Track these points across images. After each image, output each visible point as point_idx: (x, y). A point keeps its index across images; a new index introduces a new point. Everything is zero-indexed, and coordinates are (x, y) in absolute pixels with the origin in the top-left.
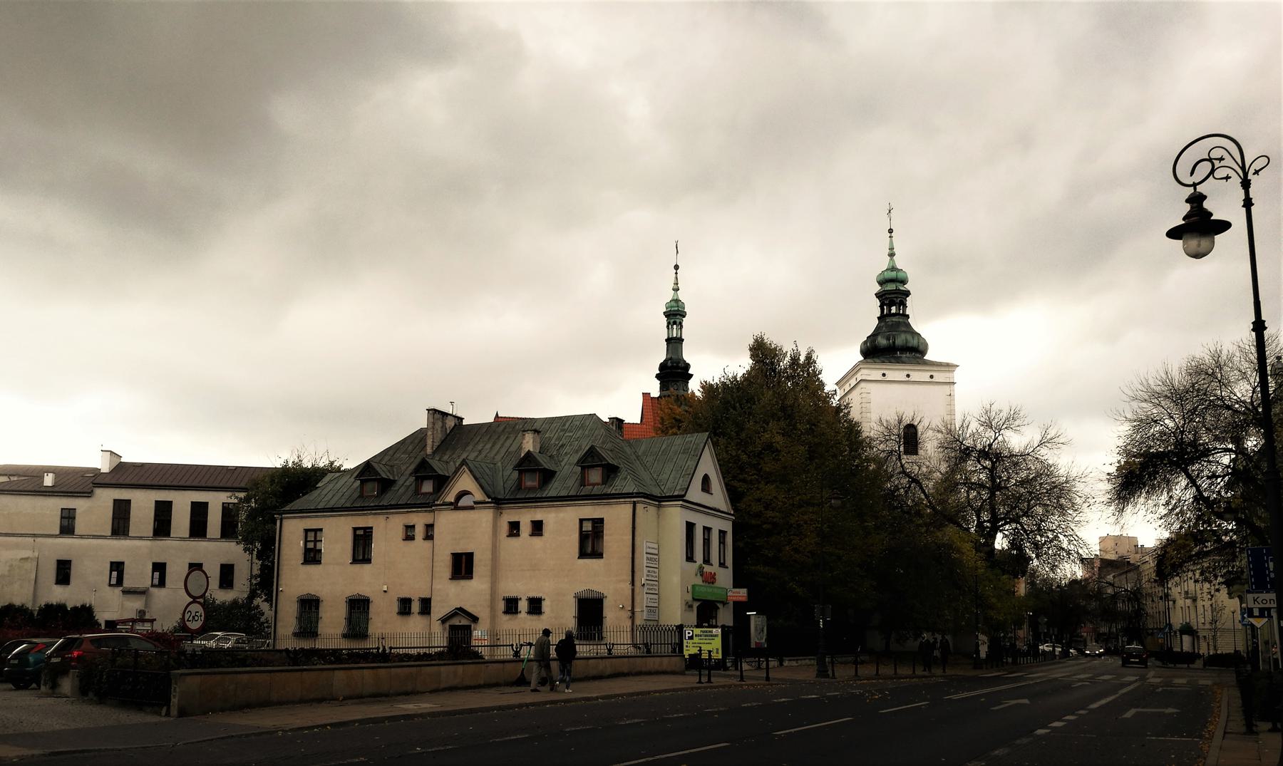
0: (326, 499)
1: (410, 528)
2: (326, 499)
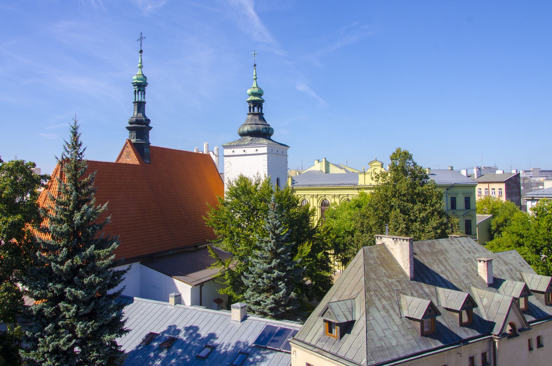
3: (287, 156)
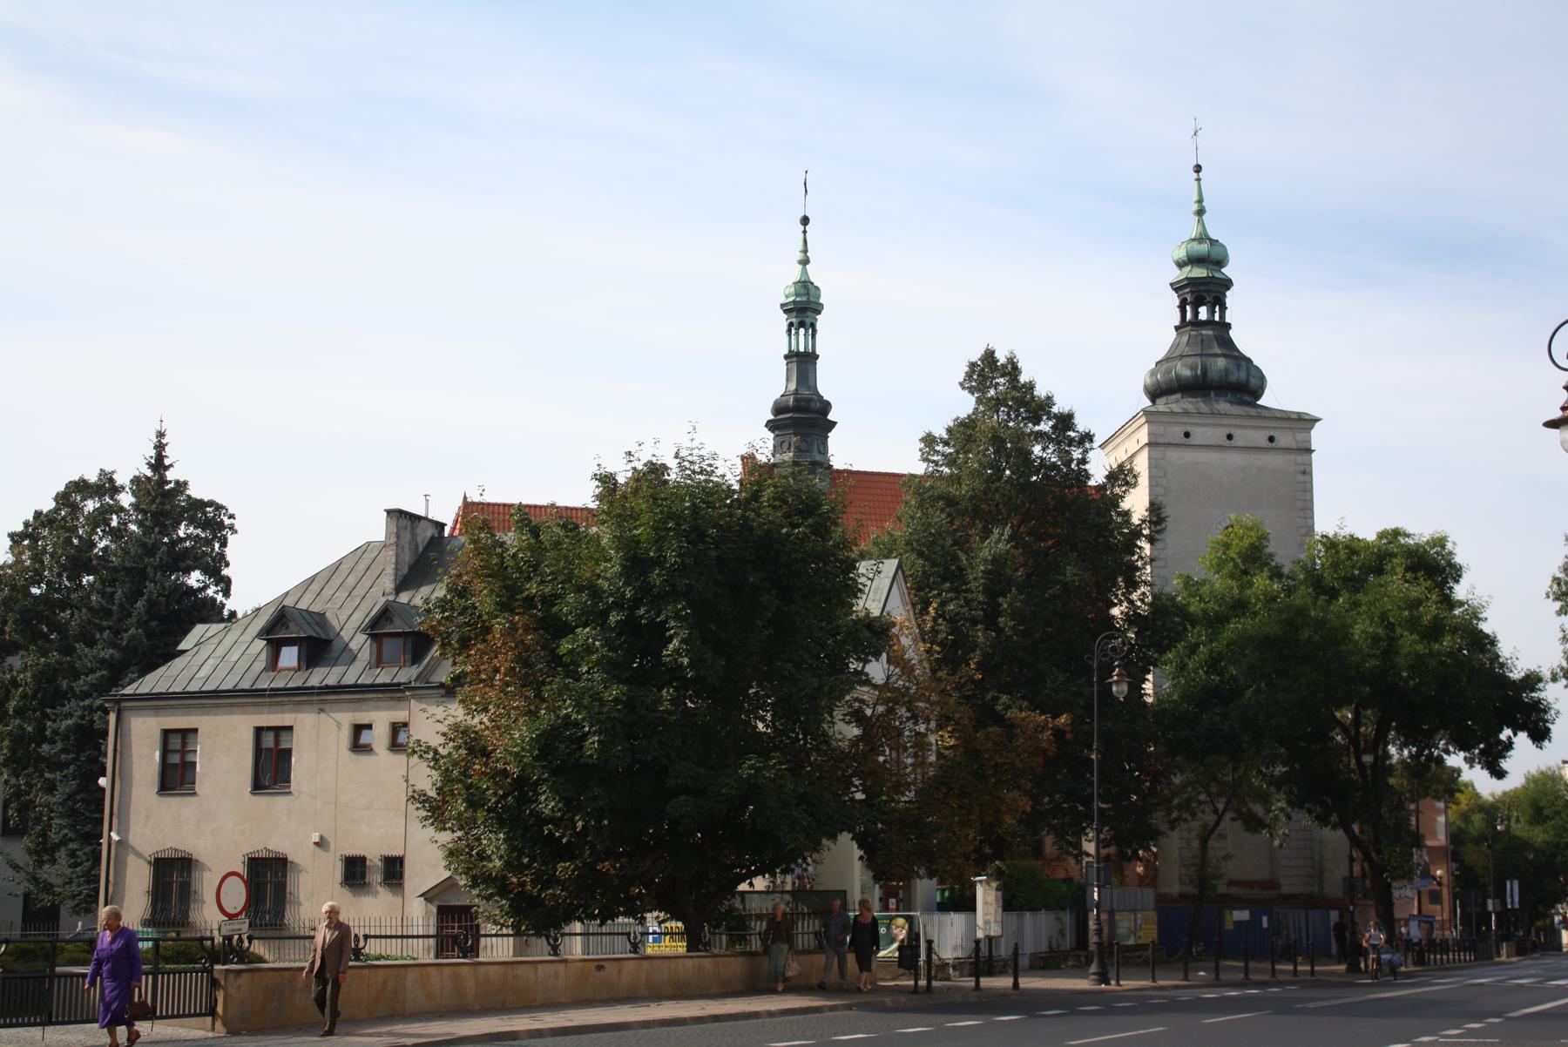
0: (202, 673)
1: (358, 729)
2: (202, 673)
3: (1310, 451)
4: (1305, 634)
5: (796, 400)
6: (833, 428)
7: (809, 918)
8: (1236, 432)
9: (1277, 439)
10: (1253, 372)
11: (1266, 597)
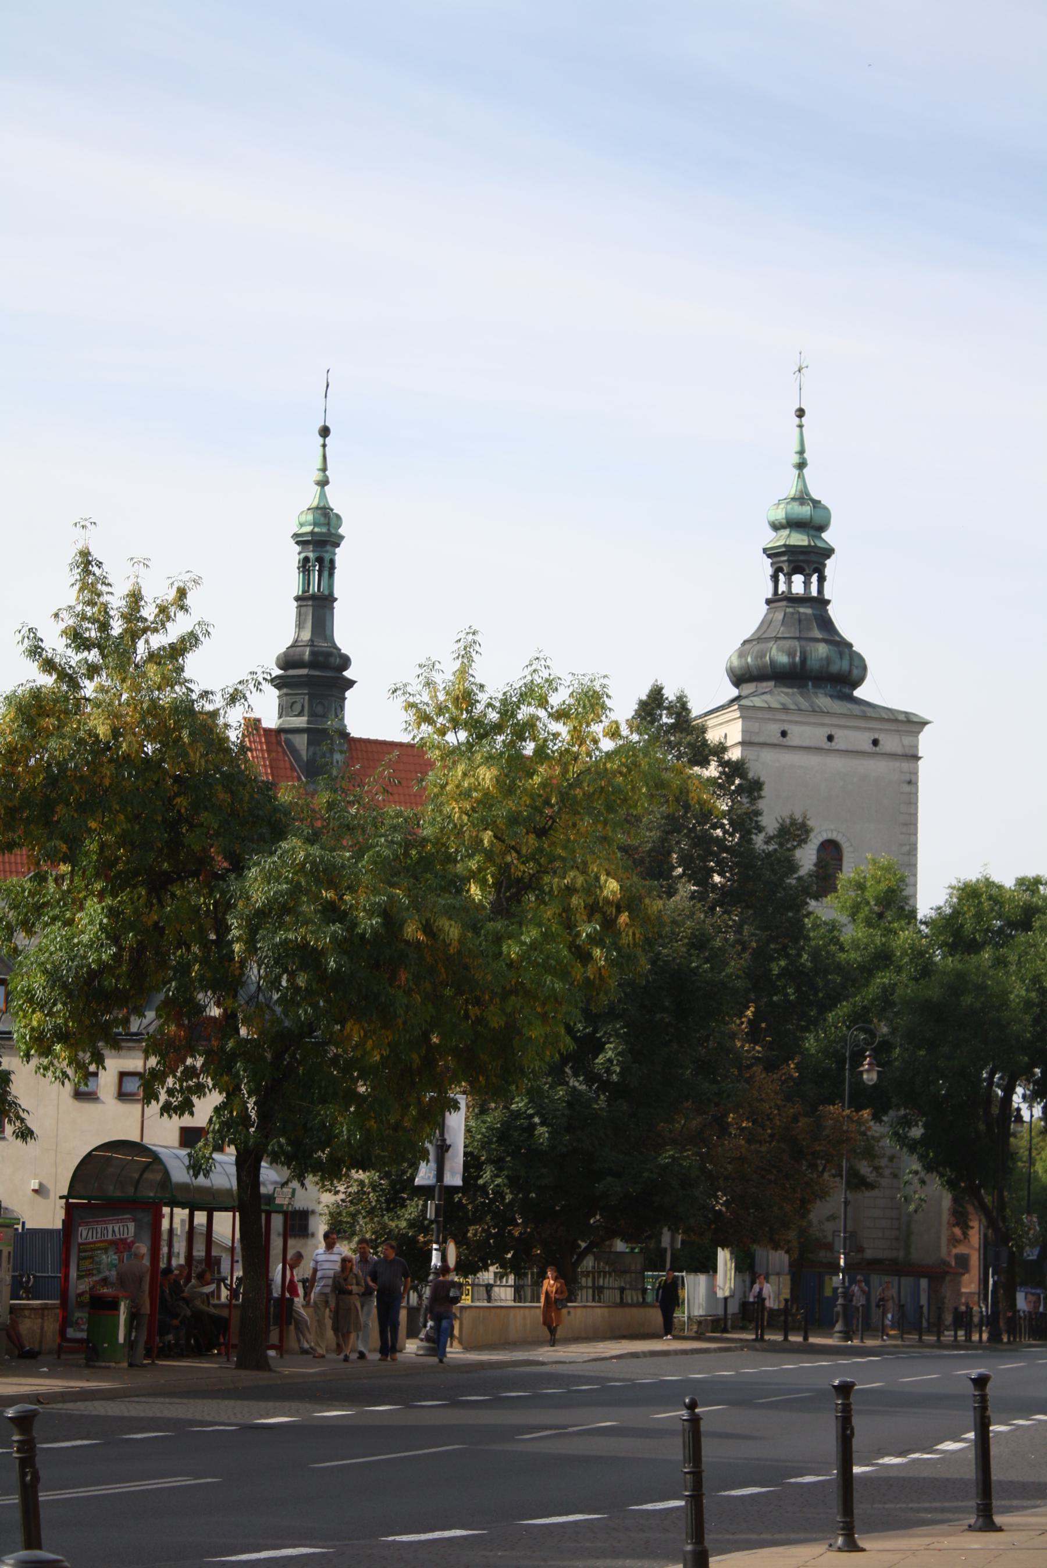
3: (916, 758)
4: (967, 1000)
5: (312, 653)
6: (351, 687)
7: (610, 1275)
8: (838, 733)
9: (881, 742)
10: (856, 662)
11: (913, 951)
